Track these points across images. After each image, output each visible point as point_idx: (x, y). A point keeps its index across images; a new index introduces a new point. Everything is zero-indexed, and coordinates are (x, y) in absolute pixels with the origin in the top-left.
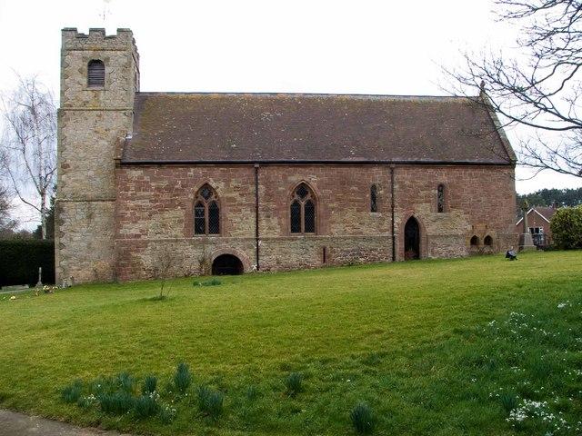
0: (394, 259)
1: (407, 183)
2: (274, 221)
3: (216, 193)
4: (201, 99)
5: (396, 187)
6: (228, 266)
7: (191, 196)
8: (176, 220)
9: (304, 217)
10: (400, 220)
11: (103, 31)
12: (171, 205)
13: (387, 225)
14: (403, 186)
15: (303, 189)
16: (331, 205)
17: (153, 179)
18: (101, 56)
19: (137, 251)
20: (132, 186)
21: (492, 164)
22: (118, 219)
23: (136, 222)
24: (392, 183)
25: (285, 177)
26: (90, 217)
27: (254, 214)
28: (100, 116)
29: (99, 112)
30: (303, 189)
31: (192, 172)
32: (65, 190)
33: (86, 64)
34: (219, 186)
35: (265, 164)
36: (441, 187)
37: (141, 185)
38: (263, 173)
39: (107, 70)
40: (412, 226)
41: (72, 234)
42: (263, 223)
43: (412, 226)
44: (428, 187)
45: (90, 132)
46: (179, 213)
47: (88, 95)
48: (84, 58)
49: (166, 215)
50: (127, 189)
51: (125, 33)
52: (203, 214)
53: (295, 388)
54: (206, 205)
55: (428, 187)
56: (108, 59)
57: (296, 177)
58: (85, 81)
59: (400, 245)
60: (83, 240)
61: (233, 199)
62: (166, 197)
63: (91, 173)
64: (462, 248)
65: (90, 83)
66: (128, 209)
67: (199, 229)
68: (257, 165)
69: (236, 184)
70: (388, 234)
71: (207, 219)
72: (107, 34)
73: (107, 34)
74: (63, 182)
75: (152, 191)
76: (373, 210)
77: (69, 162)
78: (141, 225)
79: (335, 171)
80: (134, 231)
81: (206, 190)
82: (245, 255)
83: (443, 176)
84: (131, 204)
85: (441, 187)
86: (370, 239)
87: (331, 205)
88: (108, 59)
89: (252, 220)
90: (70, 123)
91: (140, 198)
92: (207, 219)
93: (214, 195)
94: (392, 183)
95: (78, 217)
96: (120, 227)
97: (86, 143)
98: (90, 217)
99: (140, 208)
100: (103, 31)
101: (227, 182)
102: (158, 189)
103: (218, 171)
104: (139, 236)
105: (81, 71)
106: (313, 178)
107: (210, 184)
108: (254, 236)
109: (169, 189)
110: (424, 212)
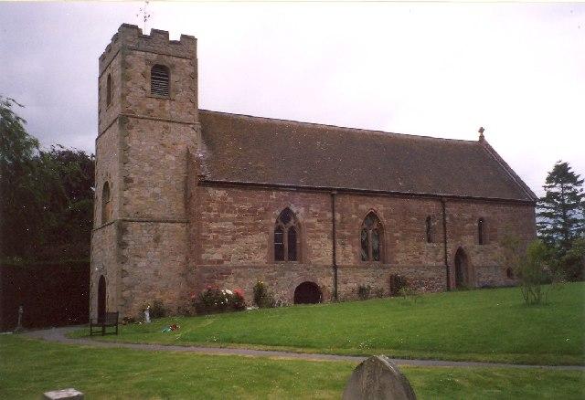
0: (448, 286)
1: (455, 215)
2: (349, 248)
3: (295, 218)
4: (312, 129)
5: (447, 219)
6: (308, 294)
7: (274, 221)
8: (256, 247)
9: (373, 252)
10: (451, 250)
11: (166, 34)
12: (255, 229)
13: (440, 256)
14: (452, 218)
15: (372, 216)
16: (395, 235)
17: (236, 201)
18: (167, 61)
19: (222, 279)
20: (214, 206)
21: (574, 365)
22: (194, 244)
23: (219, 247)
24: (444, 215)
25: (357, 206)
26: (157, 240)
27: (331, 242)
28: (167, 128)
29: (166, 124)
30: (372, 216)
31: (274, 195)
32: (127, 207)
33: (150, 67)
34: (298, 210)
35: (341, 192)
36: (481, 220)
37: (224, 207)
38: (340, 200)
39: (173, 78)
40: (461, 255)
41: (136, 259)
42: (339, 249)
43: (461, 255)
44: (472, 220)
45: (157, 144)
46: (262, 238)
47: (152, 104)
48: (148, 62)
49: (249, 239)
50: (210, 210)
51: (189, 42)
52: (282, 237)
53: (572, 12)
54: (286, 230)
55: (472, 220)
56: (173, 66)
57: (365, 207)
58: (148, 88)
59: (452, 282)
60: (148, 267)
61: (311, 225)
62: (250, 220)
63: (157, 190)
64: (501, 278)
65: (153, 90)
66: (210, 231)
67: (278, 254)
68: (335, 192)
69: (315, 211)
70: (442, 263)
71: (287, 246)
72: (172, 38)
73: (172, 38)
74: (126, 199)
75: (235, 213)
76: (429, 241)
77: (132, 176)
78: (225, 248)
79: (398, 202)
80: (217, 256)
81: (286, 215)
82: (325, 282)
83: (483, 212)
84: (214, 226)
85: (481, 220)
86: (429, 268)
87: (395, 235)
88: (173, 66)
89: (330, 247)
90: (133, 132)
91: (222, 221)
92: (287, 246)
93: (292, 220)
94: (444, 215)
95: (144, 240)
96: (203, 251)
97: (153, 157)
98: (157, 240)
99: (223, 231)
100: (166, 34)
101: (307, 207)
102: (241, 211)
103: (298, 196)
104: (220, 262)
105: (144, 75)
106: (380, 207)
107: (291, 208)
108: (330, 262)
109: (253, 211)
110: (469, 242)
